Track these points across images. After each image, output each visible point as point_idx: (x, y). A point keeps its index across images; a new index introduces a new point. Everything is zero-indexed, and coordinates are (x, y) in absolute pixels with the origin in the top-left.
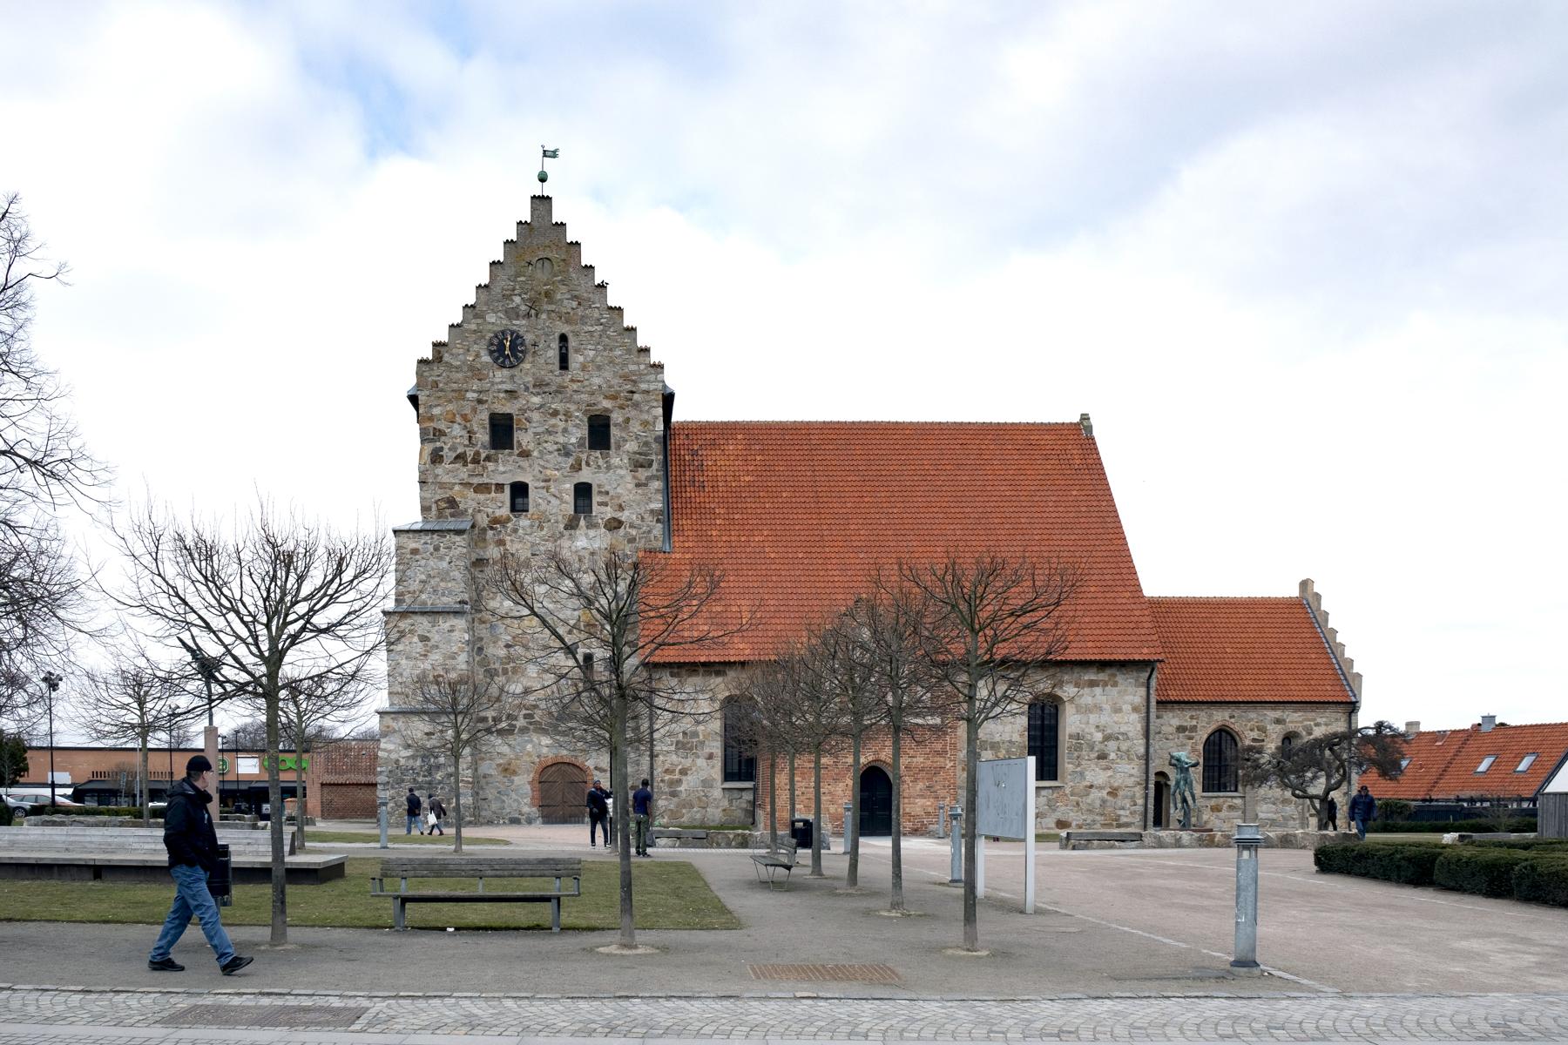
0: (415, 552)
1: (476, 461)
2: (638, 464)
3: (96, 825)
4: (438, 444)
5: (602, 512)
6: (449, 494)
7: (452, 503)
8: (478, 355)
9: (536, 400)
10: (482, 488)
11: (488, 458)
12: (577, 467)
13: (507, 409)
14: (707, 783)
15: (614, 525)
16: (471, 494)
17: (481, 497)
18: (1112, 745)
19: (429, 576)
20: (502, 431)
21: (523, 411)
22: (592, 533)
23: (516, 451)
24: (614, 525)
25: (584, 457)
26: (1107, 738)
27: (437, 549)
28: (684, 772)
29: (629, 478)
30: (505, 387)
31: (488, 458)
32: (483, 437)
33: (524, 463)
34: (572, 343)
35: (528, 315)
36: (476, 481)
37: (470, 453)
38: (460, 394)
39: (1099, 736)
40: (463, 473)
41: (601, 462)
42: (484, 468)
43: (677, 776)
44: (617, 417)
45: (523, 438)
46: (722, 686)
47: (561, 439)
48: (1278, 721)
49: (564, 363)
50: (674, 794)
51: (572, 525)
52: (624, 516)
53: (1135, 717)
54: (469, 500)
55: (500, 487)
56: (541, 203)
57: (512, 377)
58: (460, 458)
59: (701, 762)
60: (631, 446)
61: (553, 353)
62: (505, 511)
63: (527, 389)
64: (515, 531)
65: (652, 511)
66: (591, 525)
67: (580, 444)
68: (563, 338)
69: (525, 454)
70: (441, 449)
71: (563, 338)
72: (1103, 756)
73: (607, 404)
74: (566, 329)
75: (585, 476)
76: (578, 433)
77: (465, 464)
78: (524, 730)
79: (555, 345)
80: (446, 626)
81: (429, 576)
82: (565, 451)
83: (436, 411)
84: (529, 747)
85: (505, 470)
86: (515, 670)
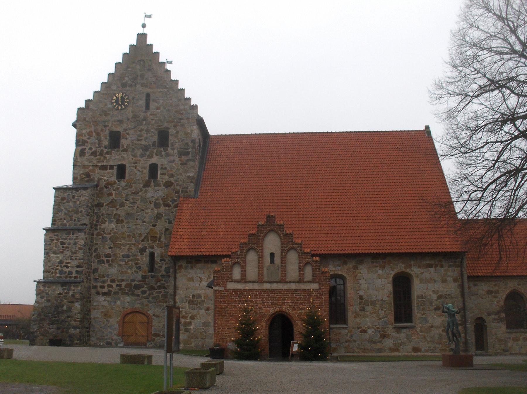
4: (84, 147)
10: (104, 168)
12: (151, 156)
13: (118, 129)
15: (168, 184)
16: (97, 170)
17: (103, 172)
20: (115, 140)
22: (157, 188)
23: (121, 149)
25: (155, 151)
26: (440, 297)
27: (74, 197)
28: (193, 318)
30: (117, 119)
31: (107, 153)
34: (152, 97)
36: (100, 164)
37: (99, 150)
39: (435, 297)
42: (105, 158)
44: (172, 131)
45: (124, 142)
49: (147, 107)
50: (187, 330)
51: (147, 185)
52: (172, 180)
55: (112, 167)
58: (94, 154)
59: (202, 312)
61: (142, 103)
62: (114, 179)
66: (157, 185)
67: (154, 145)
68: (148, 95)
69: (125, 150)
71: (148, 95)
73: (166, 125)
75: (155, 160)
77: (96, 156)
79: (144, 98)
85: (115, 158)
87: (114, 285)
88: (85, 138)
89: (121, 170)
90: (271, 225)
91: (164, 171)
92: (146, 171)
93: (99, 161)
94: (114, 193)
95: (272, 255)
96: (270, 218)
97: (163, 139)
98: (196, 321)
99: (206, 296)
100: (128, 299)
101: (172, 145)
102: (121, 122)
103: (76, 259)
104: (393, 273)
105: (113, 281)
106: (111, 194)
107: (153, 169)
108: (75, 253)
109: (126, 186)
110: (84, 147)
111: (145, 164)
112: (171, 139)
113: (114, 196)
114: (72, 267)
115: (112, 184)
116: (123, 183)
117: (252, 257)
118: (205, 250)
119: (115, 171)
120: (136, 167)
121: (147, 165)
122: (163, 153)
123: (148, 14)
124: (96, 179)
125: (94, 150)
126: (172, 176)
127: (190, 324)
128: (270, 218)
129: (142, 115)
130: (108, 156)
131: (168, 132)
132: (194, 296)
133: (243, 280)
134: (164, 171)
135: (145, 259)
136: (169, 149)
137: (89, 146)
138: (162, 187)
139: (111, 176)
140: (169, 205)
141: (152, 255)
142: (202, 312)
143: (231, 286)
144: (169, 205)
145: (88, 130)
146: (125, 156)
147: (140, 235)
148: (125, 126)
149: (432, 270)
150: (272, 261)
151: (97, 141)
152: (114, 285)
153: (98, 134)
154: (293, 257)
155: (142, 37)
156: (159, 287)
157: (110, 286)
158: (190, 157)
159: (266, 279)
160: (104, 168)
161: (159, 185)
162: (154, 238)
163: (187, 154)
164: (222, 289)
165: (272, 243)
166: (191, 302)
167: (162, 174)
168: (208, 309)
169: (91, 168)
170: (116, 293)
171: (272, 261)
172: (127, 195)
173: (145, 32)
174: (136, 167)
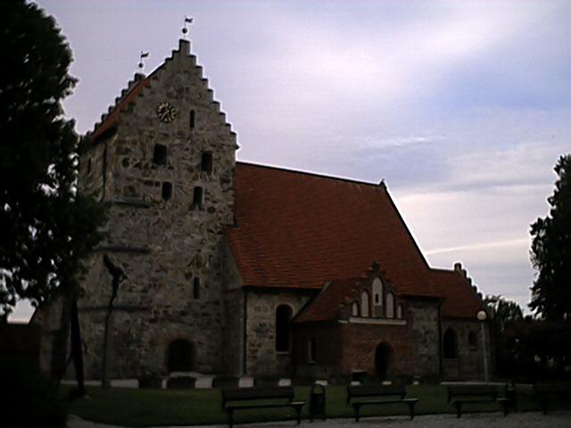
0: (121, 215)
1: (146, 167)
2: (224, 181)
3: (380, 422)
4: (127, 156)
5: (206, 204)
6: (131, 184)
7: (131, 188)
8: (151, 113)
9: (177, 141)
10: (149, 183)
11: (152, 167)
12: (195, 179)
13: (163, 143)
14: (270, 352)
15: (211, 210)
16: (142, 185)
17: (147, 187)
18: (428, 336)
19: (128, 229)
20: (160, 154)
21: (171, 145)
22: (201, 213)
23: (168, 166)
24: (211, 210)
25: (199, 174)
26: (426, 333)
27: (134, 214)
28: (259, 345)
29: (219, 187)
30: (163, 132)
31: (152, 167)
32: (150, 155)
33: (170, 172)
34: (197, 115)
35: (177, 98)
36: (146, 179)
37: (144, 164)
38: (141, 132)
39: (423, 332)
40: (139, 173)
41: (207, 177)
42: (150, 172)
43: (256, 348)
44: (215, 155)
45: (171, 159)
46: (277, 302)
47: (189, 163)
48: (468, 327)
49: (192, 125)
50: (255, 358)
51: (192, 208)
52: (216, 206)
53: (435, 323)
54: (142, 189)
55: (157, 184)
56: (184, 44)
57: (167, 128)
58: (138, 166)
59: (267, 340)
60: (220, 171)
61: (187, 119)
62: (159, 198)
63: (174, 134)
64: (164, 208)
65: (229, 206)
66: (201, 209)
67: (198, 167)
68: (192, 113)
69: (171, 168)
70: (128, 159)
71: (192, 113)
72: (425, 341)
73: (210, 148)
74: (194, 108)
75: (198, 183)
76: (197, 162)
77: (140, 168)
78: (163, 320)
79: (188, 115)
80: (139, 258)
81: (128, 229)
82: (190, 170)
83: (128, 138)
84: (165, 330)
85: (160, 175)
86: (160, 285)
87: (161, 312)
88: (129, 147)
89: (167, 189)
90: (376, 270)
91: (208, 196)
92: (191, 193)
93: (144, 175)
94: (160, 213)
95: (377, 296)
96: (375, 266)
97: (206, 161)
98: (262, 348)
99: (270, 325)
100: (174, 326)
101: (215, 171)
102: (166, 136)
103: (142, 284)
104: (279, 303)
105: (160, 306)
106: (157, 214)
107: (198, 191)
108: (141, 277)
109: (173, 206)
110: (127, 156)
111: (189, 186)
112: (214, 164)
113: (160, 215)
114: (137, 292)
115: (158, 203)
116: (169, 203)
117: (365, 296)
118: (270, 282)
119: (160, 188)
120: (181, 188)
121: (192, 187)
122: (207, 177)
123: (189, 18)
124: (142, 194)
125: (138, 161)
126: (215, 202)
127: (256, 351)
128: (375, 266)
129: (187, 132)
130: (154, 171)
131: (211, 156)
132: (260, 325)
133: (359, 315)
134: (208, 196)
135: (189, 284)
136: (212, 173)
137: (133, 156)
138: (206, 212)
139: (155, 194)
140: (212, 231)
141: (196, 281)
142: (267, 340)
143: (352, 320)
144: (212, 231)
145: (132, 138)
146: (171, 173)
147: (186, 260)
148: (170, 141)
149: (422, 310)
150: (377, 301)
151: (141, 152)
152: (161, 312)
153: (142, 144)
154: (390, 298)
155: (184, 44)
156: (204, 314)
157: (156, 312)
158: (231, 184)
159: (374, 316)
160: (149, 183)
161: (204, 210)
162: (199, 265)
163: (228, 182)
164: (346, 322)
165: (377, 286)
166: (258, 331)
167: (206, 199)
168: (271, 337)
169: (135, 181)
170: (163, 320)
171: (377, 301)
172: (173, 216)
173: (187, 39)
174: (181, 188)
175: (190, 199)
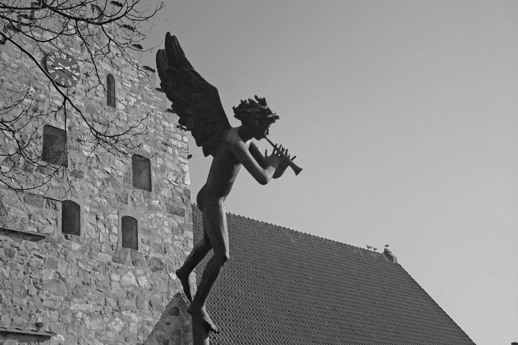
44: (156, 163)
49: (111, 101)
75: (129, 211)
107: (129, 224)
175: (116, 239)
